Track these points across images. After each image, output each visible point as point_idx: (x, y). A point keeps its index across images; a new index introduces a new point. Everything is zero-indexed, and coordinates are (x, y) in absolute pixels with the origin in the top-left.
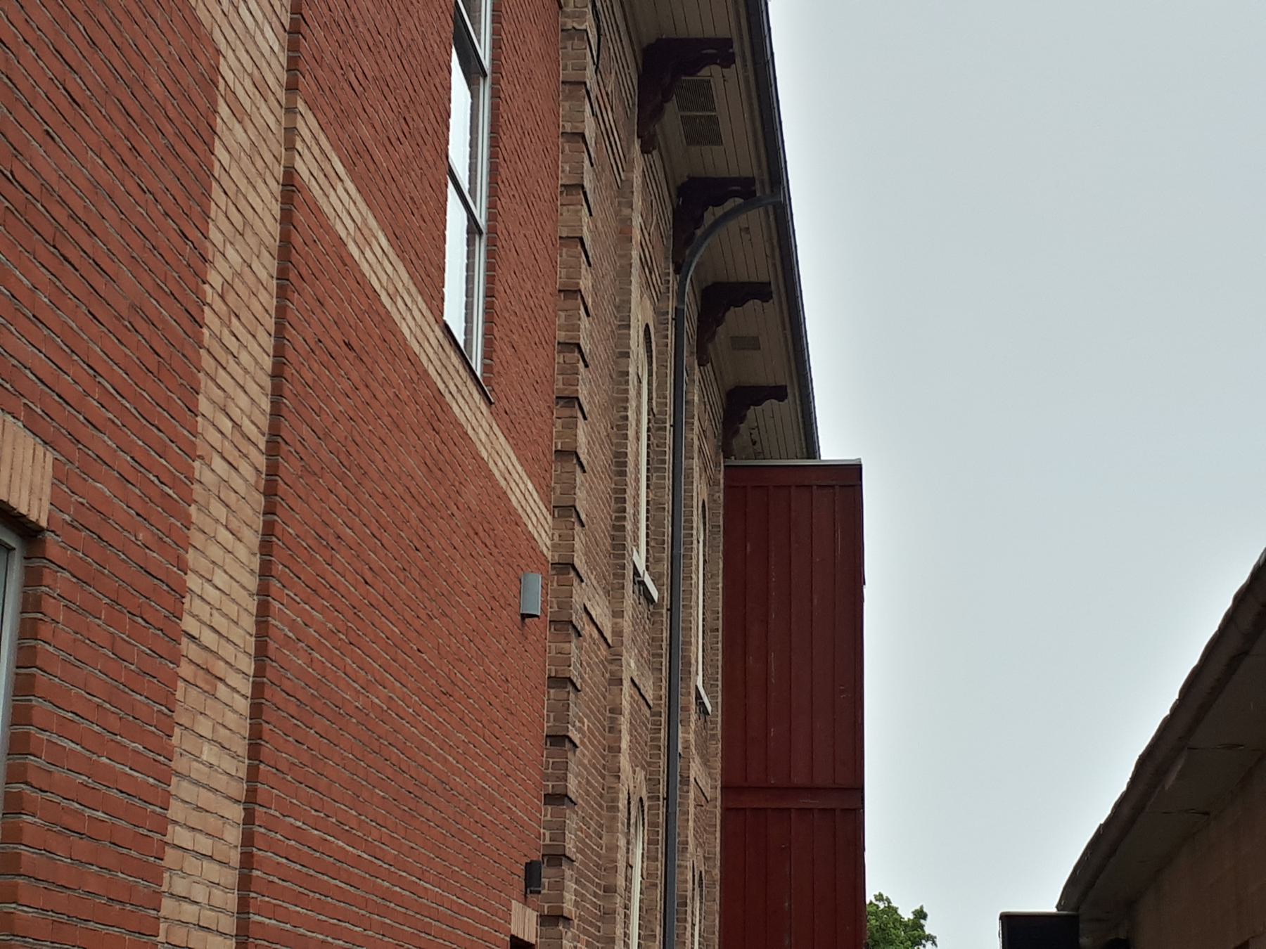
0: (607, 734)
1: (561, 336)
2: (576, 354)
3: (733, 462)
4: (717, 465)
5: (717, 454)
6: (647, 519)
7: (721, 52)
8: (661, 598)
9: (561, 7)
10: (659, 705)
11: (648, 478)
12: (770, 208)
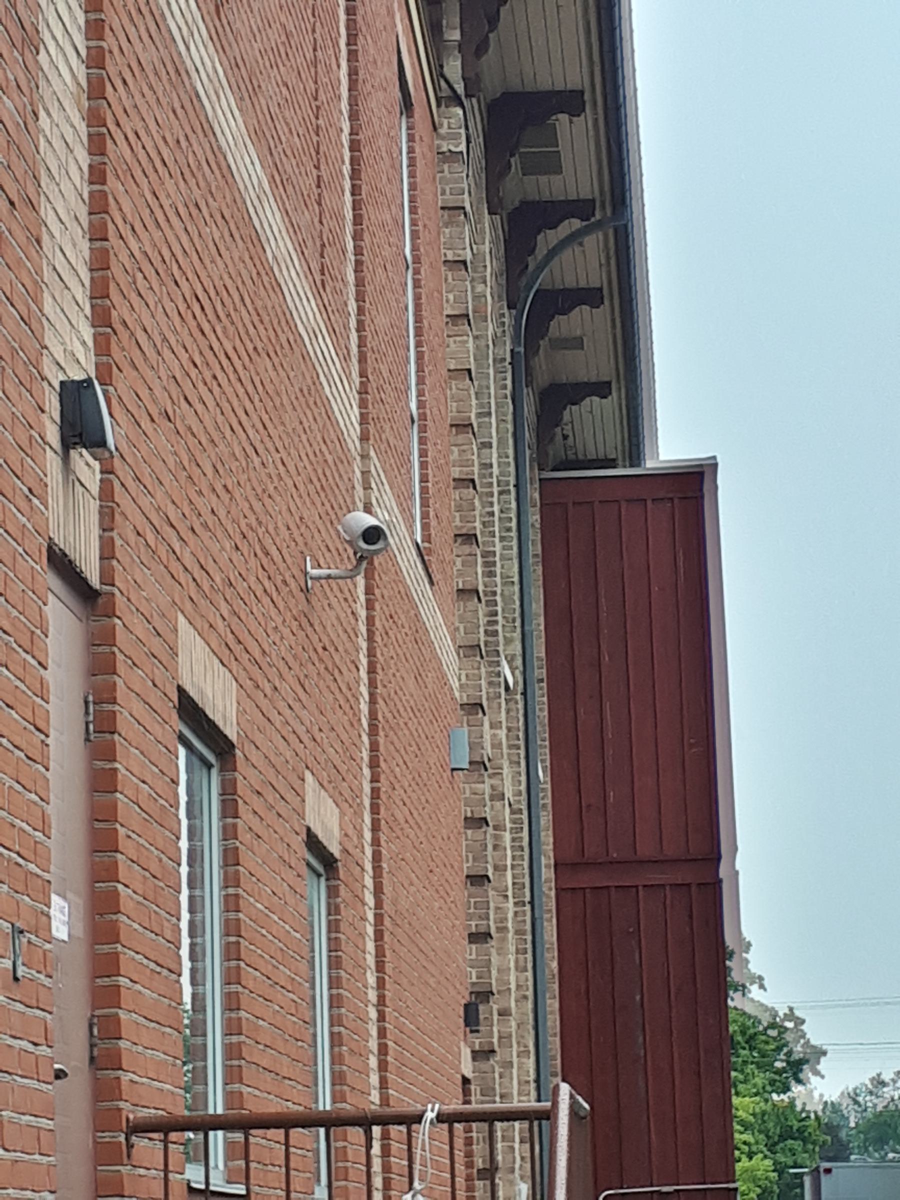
1: (456, 472)
2: (471, 490)
7: (571, 102)
12: (611, 232)
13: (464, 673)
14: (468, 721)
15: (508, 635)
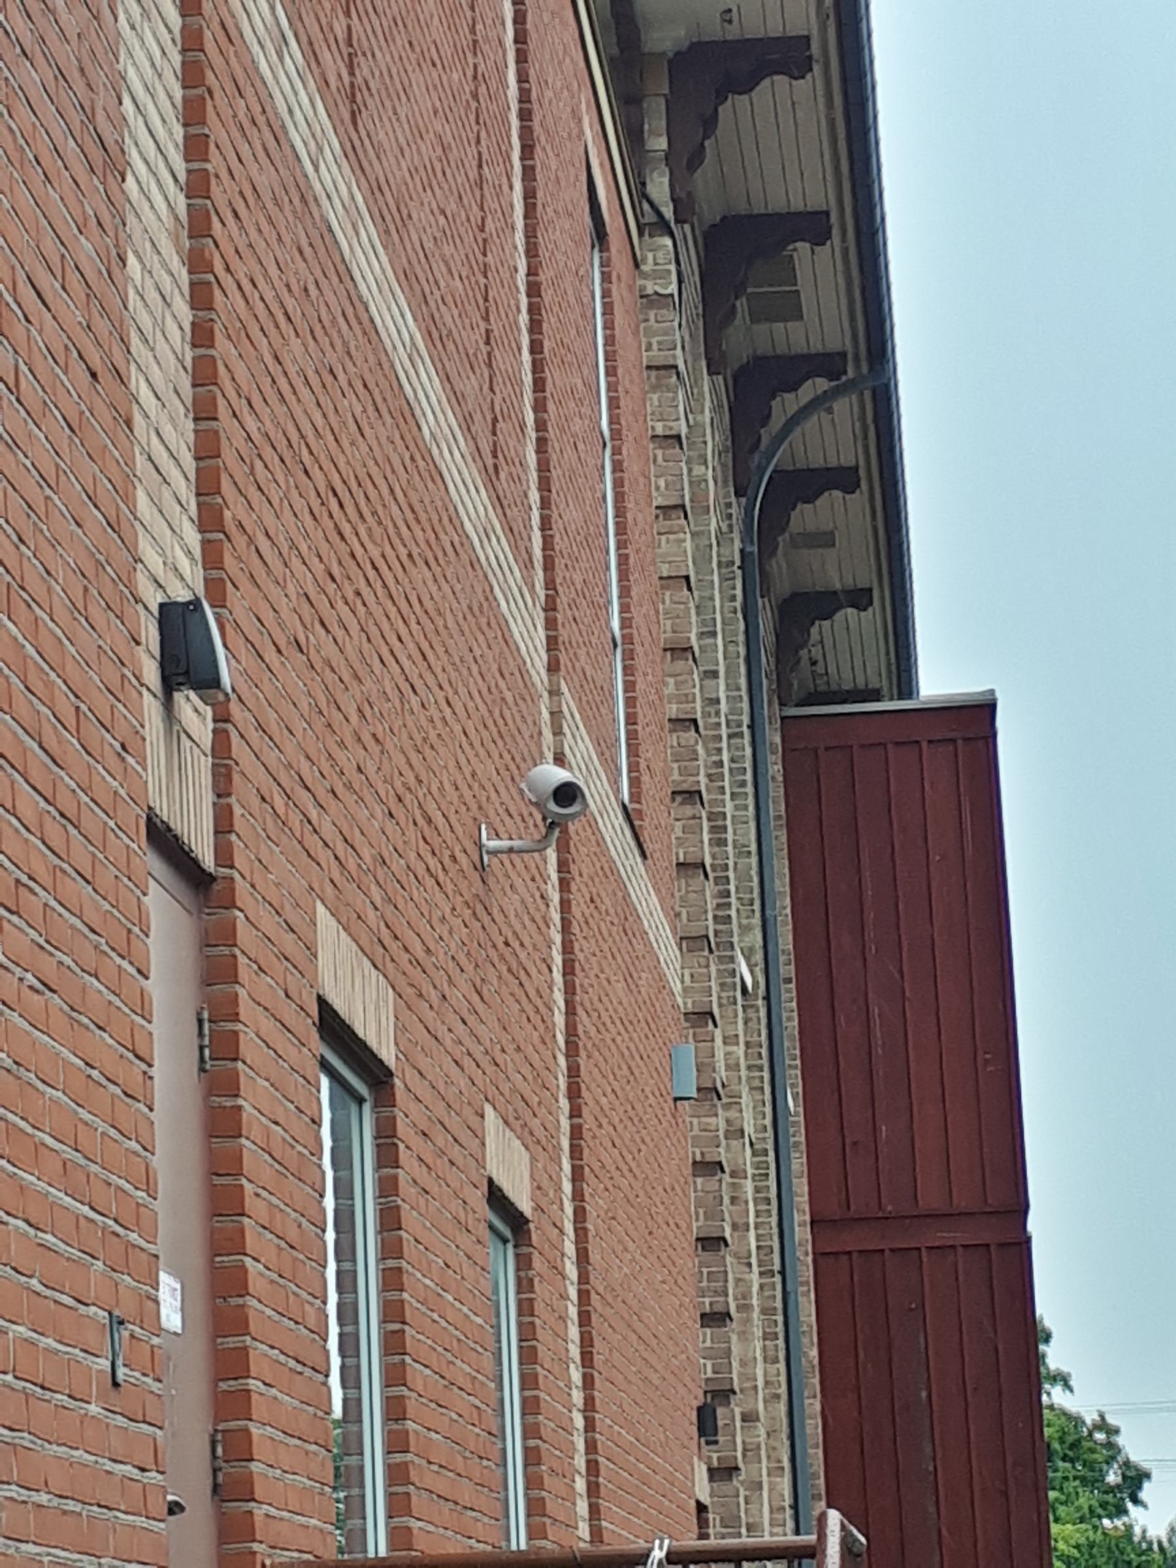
1: (673, 710)
2: (693, 733)
8: (756, 984)
9: (637, 265)
12: (867, 395)
13: (687, 972)
14: (694, 1034)
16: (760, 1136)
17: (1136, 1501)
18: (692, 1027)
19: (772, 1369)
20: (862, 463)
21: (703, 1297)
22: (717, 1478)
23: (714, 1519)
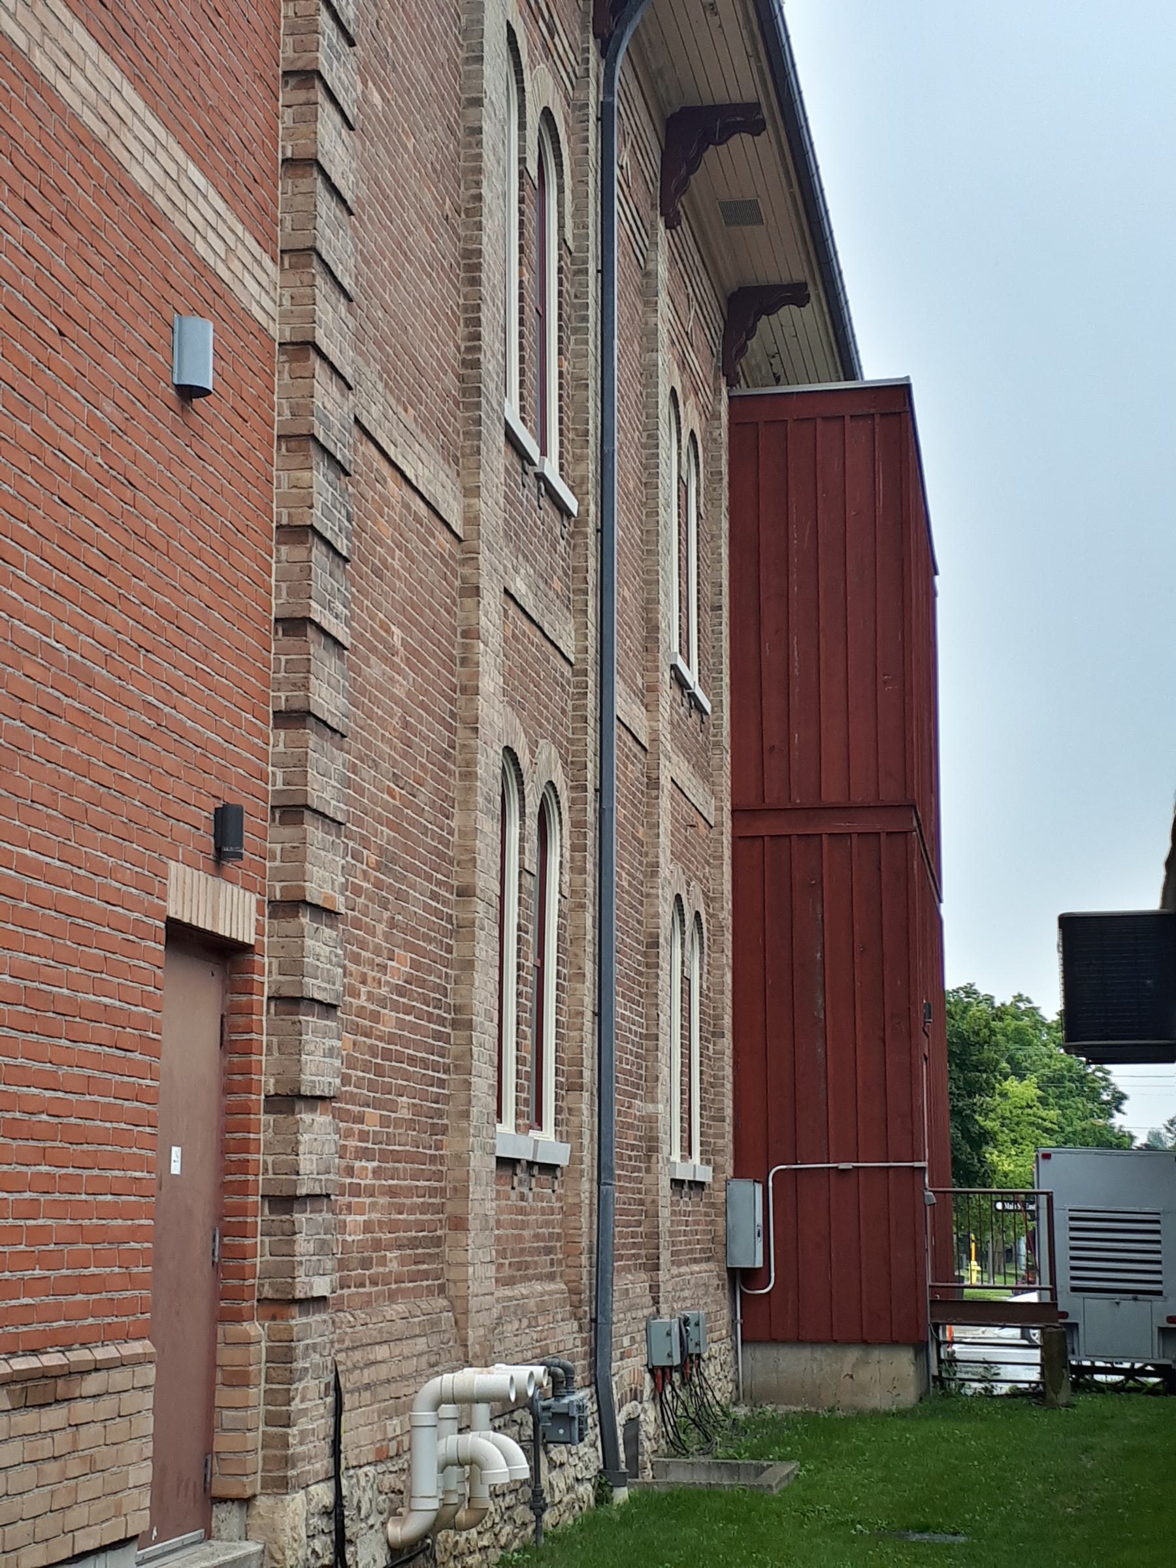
0: (458, 669)
3: (742, 390)
4: (717, 392)
5: (716, 378)
6: (561, 397)
10: (585, 660)
11: (560, 339)
13: (287, 294)
14: (290, 370)
15: (578, 451)
16: (580, 656)
17: (1119, 1111)
18: (290, 361)
19: (578, 879)
20: (762, 100)
21: (279, 690)
22: (280, 914)
23: (270, 964)
